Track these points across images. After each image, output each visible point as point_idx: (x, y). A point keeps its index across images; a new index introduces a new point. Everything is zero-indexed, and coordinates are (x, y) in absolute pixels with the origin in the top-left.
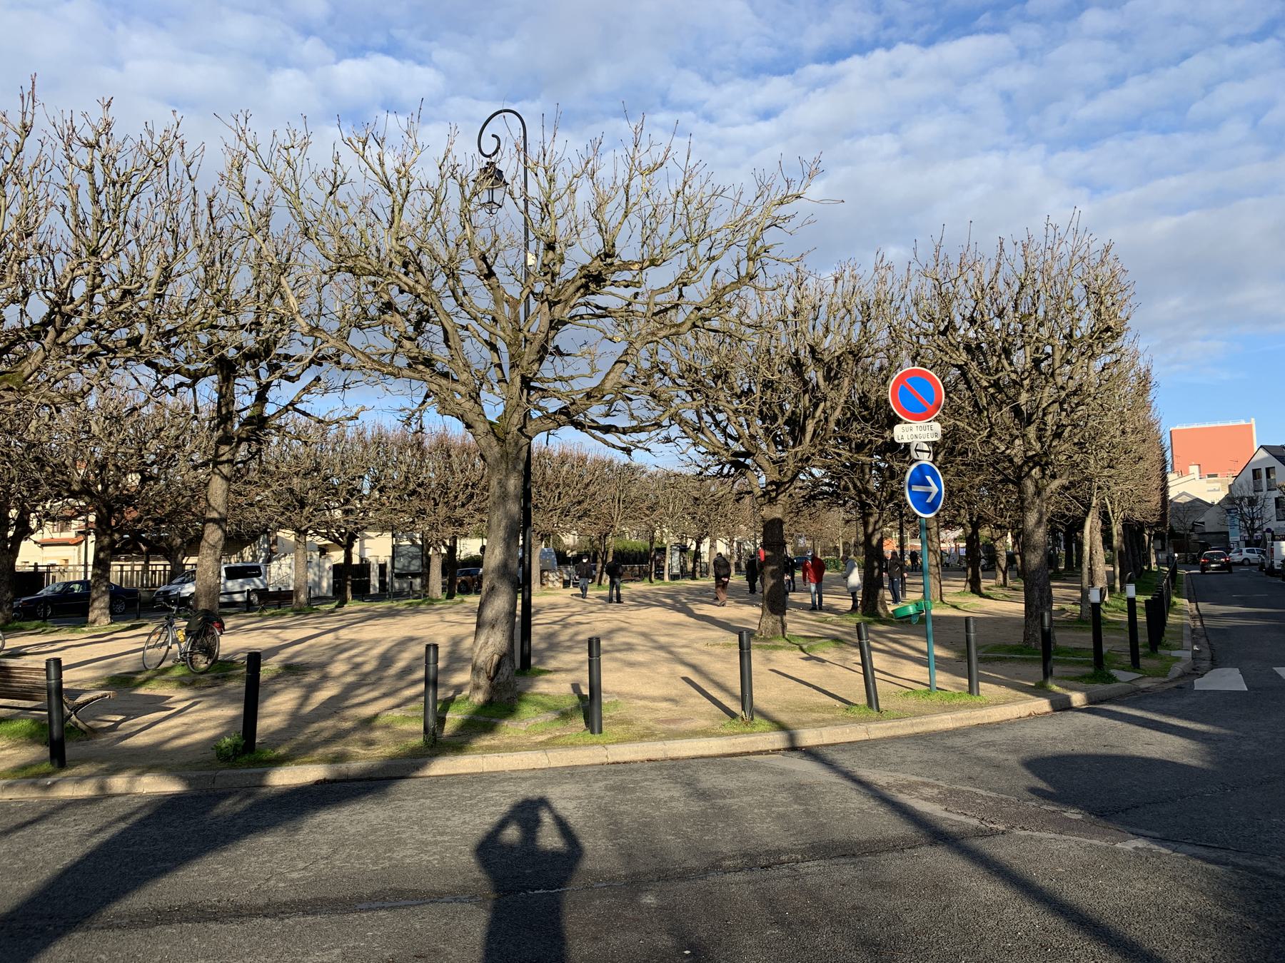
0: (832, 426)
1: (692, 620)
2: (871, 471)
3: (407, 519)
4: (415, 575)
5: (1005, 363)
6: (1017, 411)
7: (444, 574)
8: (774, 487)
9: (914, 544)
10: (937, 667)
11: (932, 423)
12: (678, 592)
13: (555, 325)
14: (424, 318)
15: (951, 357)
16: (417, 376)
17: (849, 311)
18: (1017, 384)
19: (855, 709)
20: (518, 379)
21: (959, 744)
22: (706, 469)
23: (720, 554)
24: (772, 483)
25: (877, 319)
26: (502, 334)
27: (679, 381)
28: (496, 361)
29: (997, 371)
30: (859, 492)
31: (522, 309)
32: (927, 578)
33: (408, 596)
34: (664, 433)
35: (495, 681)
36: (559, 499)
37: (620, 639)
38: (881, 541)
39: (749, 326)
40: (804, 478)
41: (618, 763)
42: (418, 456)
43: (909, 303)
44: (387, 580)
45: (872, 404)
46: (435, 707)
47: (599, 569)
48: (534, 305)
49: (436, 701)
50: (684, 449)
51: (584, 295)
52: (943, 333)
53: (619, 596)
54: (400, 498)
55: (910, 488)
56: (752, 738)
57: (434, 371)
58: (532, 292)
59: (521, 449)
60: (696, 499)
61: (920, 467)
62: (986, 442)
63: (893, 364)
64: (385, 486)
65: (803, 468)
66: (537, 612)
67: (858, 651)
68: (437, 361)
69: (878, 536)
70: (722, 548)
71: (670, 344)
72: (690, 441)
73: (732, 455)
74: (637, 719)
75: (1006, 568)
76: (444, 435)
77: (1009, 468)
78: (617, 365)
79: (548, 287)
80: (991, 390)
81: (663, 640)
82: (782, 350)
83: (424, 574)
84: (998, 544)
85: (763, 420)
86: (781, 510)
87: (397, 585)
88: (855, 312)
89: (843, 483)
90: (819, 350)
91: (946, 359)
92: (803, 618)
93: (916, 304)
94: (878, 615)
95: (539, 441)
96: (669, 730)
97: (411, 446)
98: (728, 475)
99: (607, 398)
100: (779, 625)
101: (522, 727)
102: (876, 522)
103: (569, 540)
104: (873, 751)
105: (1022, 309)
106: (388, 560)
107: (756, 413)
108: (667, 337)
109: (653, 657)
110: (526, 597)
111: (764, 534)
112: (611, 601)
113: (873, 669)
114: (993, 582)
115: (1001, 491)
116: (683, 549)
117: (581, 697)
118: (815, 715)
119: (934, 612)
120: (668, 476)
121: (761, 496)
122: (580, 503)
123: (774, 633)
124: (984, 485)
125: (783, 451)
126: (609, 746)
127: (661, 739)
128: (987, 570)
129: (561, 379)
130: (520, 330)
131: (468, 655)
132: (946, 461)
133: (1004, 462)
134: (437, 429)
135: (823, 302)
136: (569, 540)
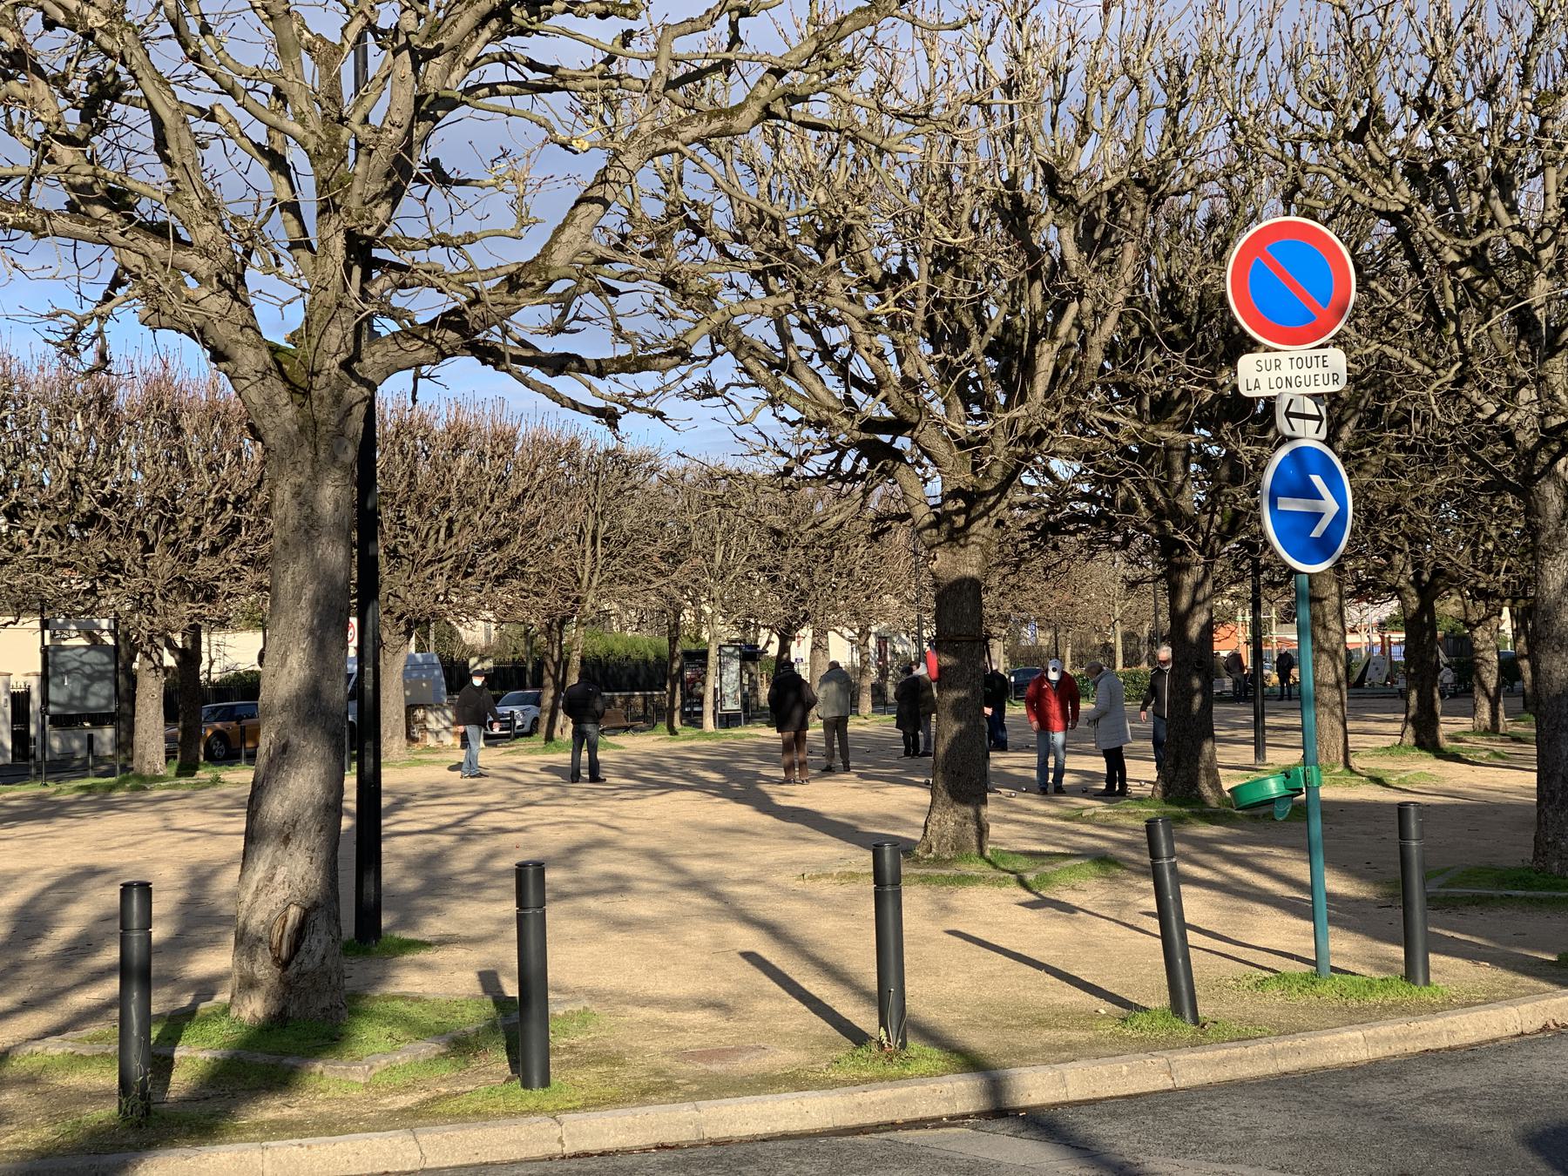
0: (1096, 357)
1: (768, 820)
2: (1186, 466)
3: (78, 583)
4: (99, 720)
5: (1499, 207)
6: (1524, 321)
7: (170, 715)
8: (961, 504)
9: (1283, 636)
10: (1332, 921)
11: (1330, 351)
12: (737, 755)
13: (429, 108)
14: (105, 91)
15: (1373, 194)
16: (88, 231)
17: (1136, 82)
18: (1525, 258)
19: (1142, 1019)
20: (339, 242)
21: (1380, 1097)
22: (801, 461)
23: (835, 666)
24: (956, 494)
25: (1202, 101)
26: (297, 129)
27: (734, 249)
28: (285, 195)
29: (1480, 227)
30: (1159, 515)
31: (347, 69)
32: (1310, 715)
33: (83, 771)
34: (698, 376)
35: (293, 969)
36: (449, 534)
37: (596, 865)
38: (1208, 630)
39: (899, 116)
40: (1033, 482)
41: (587, 1155)
42: (100, 430)
43: (1278, 63)
44: (33, 730)
45: (1190, 308)
46: (146, 1032)
47: (547, 701)
48: (377, 59)
49: (147, 1019)
50: (748, 413)
51: (500, 35)
52: (1357, 136)
53: (594, 767)
54: (59, 533)
55: (1273, 503)
56: (903, 1091)
57: (131, 219)
58: (371, 27)
59: (349, 412)
60: (779, 533)
61: (1296, 453)
62: (1453, 394)
63: (1239, 209)
64: (20, 505)
65: (1028, 457)
66: (399, 805)
67: (1149, 884)
68: (140, 195)
69: (1201, 618)
70: (841, 651)
71: (711, 159)
72: (762, 393)
73: (863, 428)
74: (633, 1051)
75: (1497, 690)
76: (165, 378)
77: (1506, 456)
78: (582, 209)
79: (410, 15)
80: (1466, 273)
81: (699, 867)
82: (979, 174)
83: (122, 716)
84: (1479, 633)
85: (936, 342)
86: (977, 558)
87: (56, 743)
88: (1151, 85)
89: (1122, 494)
90: (1065, 177)
91: (1362, 198)
92: (1028, 811)
93: (1294, 67)
94: (1200, 800)
95: (393, 392)
96: (708, 1074)
97: (84, 407)
98: (853, 476)
99: (557, 288)
100: (972, 827)
101: (359, 1075)
102: (1198, 585)
103: (476, 633)
104: (1181, 1116)
105: (1539, 80)
106: (34, 683)
107: (918, 326)
108: (704, 141)
109: (674, 907)
110: (369, 767)
111: (938, 619)
112: (575, 777)
113: (1184, 927)
114: (1466, 723)
115: (1487, 510)
116: (750, 654)
117: (501, 1001)
118: (1049, 1035)
119: (1327, 793)
120: (712, 478)
121: (931, 525)
122: (499, 544)
123: (958, 846)
124: (1449, 496)
125: (983, 417)
126: (564, 1117)
127: (690, 1097)
128: (1454, 696)
129: (444, 241)
130: (342, 120)
131: (228, 909)
132: (1361, 440)
133: (1494, 441)
134: (147, 364)
135: (1075, 60)
136: (476, 633)
